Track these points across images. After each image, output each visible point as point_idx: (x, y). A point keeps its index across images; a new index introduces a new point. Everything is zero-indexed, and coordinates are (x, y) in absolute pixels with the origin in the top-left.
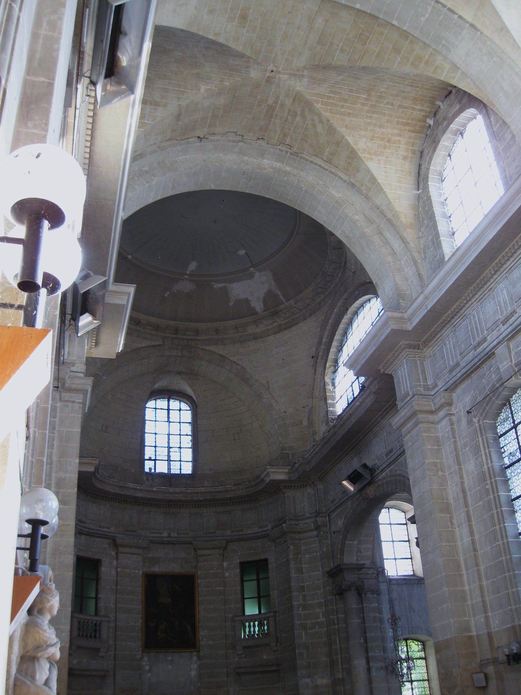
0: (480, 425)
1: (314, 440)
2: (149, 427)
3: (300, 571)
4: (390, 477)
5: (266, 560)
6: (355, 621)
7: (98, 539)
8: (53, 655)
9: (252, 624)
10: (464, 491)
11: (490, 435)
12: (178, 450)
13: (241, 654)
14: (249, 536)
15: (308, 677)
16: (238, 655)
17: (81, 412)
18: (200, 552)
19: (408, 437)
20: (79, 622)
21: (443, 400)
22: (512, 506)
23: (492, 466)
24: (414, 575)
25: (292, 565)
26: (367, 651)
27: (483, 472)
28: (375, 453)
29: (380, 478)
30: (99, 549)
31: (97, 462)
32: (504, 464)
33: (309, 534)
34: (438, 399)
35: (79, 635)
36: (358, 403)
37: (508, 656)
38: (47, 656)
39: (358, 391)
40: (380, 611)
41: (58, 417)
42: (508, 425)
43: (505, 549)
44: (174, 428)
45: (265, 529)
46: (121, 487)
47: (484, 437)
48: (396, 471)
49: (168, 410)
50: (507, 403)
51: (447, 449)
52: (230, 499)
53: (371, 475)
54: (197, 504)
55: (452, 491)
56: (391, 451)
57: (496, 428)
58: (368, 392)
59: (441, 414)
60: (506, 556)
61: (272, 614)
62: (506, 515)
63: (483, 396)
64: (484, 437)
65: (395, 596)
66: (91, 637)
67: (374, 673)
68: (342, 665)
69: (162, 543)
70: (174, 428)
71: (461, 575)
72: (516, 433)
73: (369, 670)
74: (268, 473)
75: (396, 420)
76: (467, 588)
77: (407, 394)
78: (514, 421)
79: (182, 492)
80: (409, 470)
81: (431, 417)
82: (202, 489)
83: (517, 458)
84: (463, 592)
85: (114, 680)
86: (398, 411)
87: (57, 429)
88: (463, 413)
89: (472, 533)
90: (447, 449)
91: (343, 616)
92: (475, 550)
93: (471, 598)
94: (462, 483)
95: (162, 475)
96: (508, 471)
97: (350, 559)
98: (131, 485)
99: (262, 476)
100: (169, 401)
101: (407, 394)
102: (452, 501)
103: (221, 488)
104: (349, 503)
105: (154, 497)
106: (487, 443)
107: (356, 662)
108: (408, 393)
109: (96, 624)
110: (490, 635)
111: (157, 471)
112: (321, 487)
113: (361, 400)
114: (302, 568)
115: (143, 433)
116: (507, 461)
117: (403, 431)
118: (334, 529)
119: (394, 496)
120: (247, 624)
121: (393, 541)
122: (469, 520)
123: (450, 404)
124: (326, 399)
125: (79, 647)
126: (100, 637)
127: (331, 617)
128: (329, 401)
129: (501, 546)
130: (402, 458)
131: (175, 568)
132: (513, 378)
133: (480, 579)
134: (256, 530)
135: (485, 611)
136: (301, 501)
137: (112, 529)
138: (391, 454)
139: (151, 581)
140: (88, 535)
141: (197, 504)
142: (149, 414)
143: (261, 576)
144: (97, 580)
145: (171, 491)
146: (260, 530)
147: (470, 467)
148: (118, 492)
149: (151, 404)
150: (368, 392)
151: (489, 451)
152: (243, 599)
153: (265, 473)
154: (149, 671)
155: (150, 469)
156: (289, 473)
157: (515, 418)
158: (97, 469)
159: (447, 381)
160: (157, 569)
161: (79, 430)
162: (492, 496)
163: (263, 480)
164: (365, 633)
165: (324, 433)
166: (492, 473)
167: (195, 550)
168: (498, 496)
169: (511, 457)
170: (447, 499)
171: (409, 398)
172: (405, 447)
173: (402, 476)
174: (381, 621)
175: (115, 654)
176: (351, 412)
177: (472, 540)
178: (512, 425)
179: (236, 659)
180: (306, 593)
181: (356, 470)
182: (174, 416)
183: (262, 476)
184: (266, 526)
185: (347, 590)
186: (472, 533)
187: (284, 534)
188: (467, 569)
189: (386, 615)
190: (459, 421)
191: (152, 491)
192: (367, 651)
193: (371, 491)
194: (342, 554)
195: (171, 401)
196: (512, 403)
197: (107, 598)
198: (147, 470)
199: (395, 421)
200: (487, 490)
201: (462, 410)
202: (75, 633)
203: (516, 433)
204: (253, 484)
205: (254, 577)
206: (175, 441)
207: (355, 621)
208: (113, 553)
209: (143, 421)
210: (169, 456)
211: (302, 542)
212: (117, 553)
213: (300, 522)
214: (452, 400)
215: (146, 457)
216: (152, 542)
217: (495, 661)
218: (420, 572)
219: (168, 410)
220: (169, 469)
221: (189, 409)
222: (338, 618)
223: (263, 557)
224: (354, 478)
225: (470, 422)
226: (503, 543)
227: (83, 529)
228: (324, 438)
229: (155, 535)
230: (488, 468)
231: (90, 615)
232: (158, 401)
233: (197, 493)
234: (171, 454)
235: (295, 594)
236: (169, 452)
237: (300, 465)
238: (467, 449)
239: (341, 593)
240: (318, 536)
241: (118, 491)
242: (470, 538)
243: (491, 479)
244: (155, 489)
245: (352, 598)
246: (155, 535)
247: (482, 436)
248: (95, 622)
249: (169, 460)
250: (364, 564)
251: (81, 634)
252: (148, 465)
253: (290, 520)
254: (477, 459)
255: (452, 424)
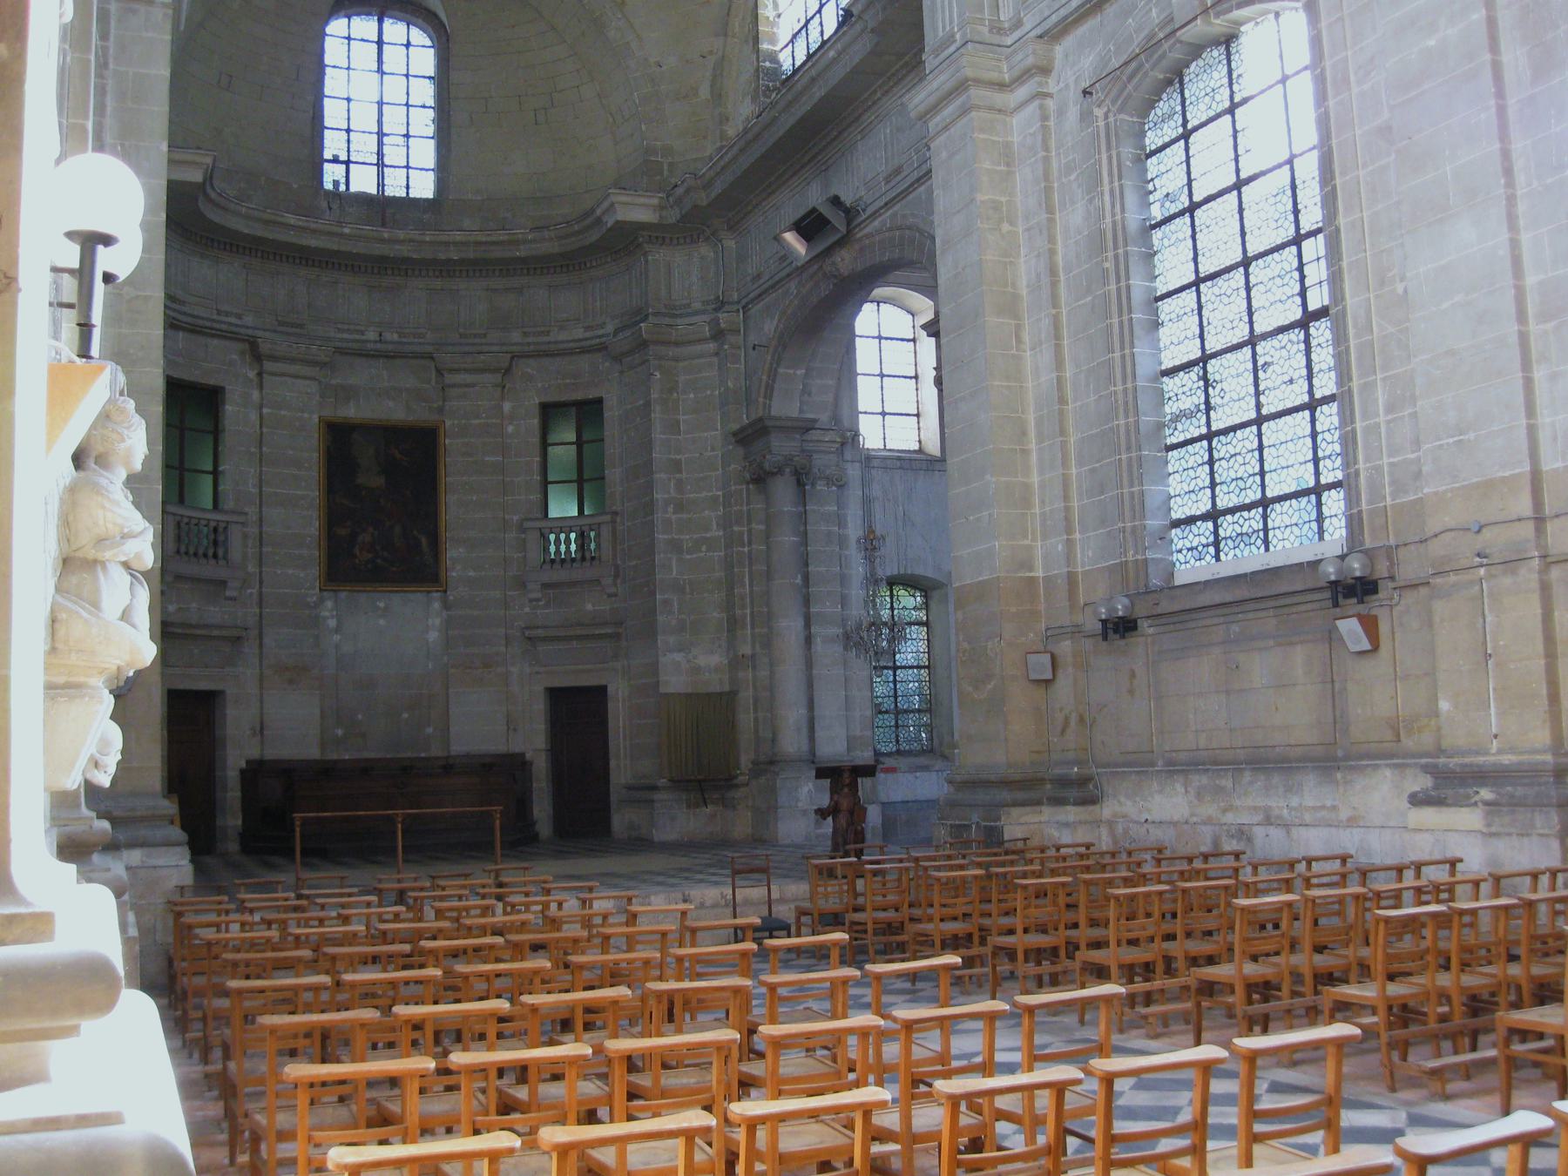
0: (1107, 125)
1: (723, 136)
2: (333, 83)
3: (674, 427)
4: (890, 229)
5: (600, 401)
6: (786, 538)
7: (216, 341)
8: (138, 556)
9: (563, 536)
10: (1053, 272)
11: (1128, 151)
12: (401, 140)
13: (538, 600)
14: (562, 346)
15: (680, 651)
16: (531, 601)
17: (168, 26)
18: (450, 378)
19: (942, 138)
20: (178, 524)
21: (1030, 60)
22: (1156, 312)
23: (1123, 219)
24: (920, 451)
25: (657, 414)
26: (807, 602)
27: (1102, 233)
28: (860, 174)
29: (866, 231)
30: (216, 364)
31: (209, 160)
32: (1149, 219)
33: (698, 348)
34: (1019, 57)
35: (178, 552)
36: (832, 54)
37: (1104, 622)
38: (123, 559)
39: (835, 25)
40: (841, 523)
41: (112, 39)
42: (1171, 130)
43: (1126, 403)
44: (394, 89)
45: (601, 332)
46: (267, 222)
47: (1114, 153)
48: (904, 216)
49: (380, 43)
50: (1176, 78)
51: (1025, 176)
52: (523, 260)
53: (848, 224)
54: (445, 269)
55: (1025, 270)
56: (898, 171)
57: (1143, 134)
58: (858, 27)
59: (1022, 92)
60: (1127, 417)
61: (607, 518)
62: (1138, 331)
63: (1124, 58)
64: (1114, 153)
65: (876, 491)
66: (205, 555)
67: (818, 646)
68: (753, 628)
69: (364, 354)
70: (394, 89)
71: (1025, 452)
72: (1187, 149)
73: (809, 640)
74: (612, 205)
75: (919, 98)
76: (1035, 479)
77: (951, 38)
78: (1185, 122)
79: (411, 241)
80: (936, 219)
81: (999, 99)
82: (458, 236)
83: (1181, 207)
84: (1027, 487)
85: (261, 645)
86: (921, 80)
87: (111, 66)
88: (1074, 94)
89: (1059, 364)
90: (1025, 176)
91: (762, 527)
92: (1062, 400)
93: (1043, 502)
94: (1052, 252)
95: (363, 198)
96: (1157, 235)
97: (784, 407)
98: (291, 219)
99: (598, 212)
100: (380, 22)
101: (951, 38)
102: (1024, 292)
103: (502, 236)
104: (792, 286)
105: (343, 248)
106: (1119, 165)
107: (783, 623)
108: (953, 36)
109: (215, 530)
110: (1071, 579)
111: (353, 189)
112: (730, 244)
113: (839, 46)
114: (678, 422)
115: (319, 96)
116: (1157, 213)
117: (931, 125)
118: (753, 339)
119: (891, 277)
120: (552, 537)
121: (882, 376)
122: (1058, 337)
123: (1045, 71)
124: (756, 40)
125: (179, 577)
126: (225, 558)
127: (736, 529)
128: (764, 46)
129: (1120, 396)
130: (922, 188)
131: (394, 411)
132: (1198, 21)
133: (1065, 463)
134: (579, 333)
135: (1069, 530)
136: (684, 274)
137: (249, 320)
138: (899, 178)
139: (341, 441)
140: (192, 331)
141: (445, 269)
142: (333, 51)
143: (586, 436)
144: (216, 432)
145: (386, 235)
146: (588, 335)
147: (1074, 218)
148: (259, 233)
149: (337, 26)
150: (858, 27)
151: (1121, 186)
152: (545, 483)
153: (606, 204)
154: (337, 630)
155: (336, 183)
156: (662, 208)
157: (1189, 116)
158: (209, 178)
159: (1047, 13)
160: (351, 412)
161: (166, 72)
162: (1113, 287)
163: (599, 221)
164: (807, 565)
165: (747, 120)
166: (1120, 233)
167: (439, 372)
168: (1128, 287)
169: (1167, 204)
170: (1014, 285)
171: (952, 49)
172: (934, 163)
173: (921, 232)
174: (842, 541)
175: (261, 594)
176: (813, 72)
177: (1059, 379)
178: (1181, 130)
179: (527, 610)
180: (684, 475)
181: (814, 210)
182: (394, 58)
183: (598, 212)
184: (602, 326)
185: (774, 474)
186: (1059, 364)
187: (644, 344)
188: (1041, 438)
189: (854, 531)
190: (1061, 112)
191: (342, 235)
192: (807, 602)
193: (845, 261)
194: (769, 391)
195: (387, 23)
196: (1186, 79)
197: (239, 472)
198: (328, 186)
199: (916, 101)
200: (1105, 272)
201: (1072, 87)
202: (172, 546)
203: (1187, 149)
204: (576, 228)
205: (572, 437)
206: (394, 120)
207: (786, 538)
208: (252, 374)
209: (321, 67)
210: (380, 154)
211: (681, 364)
212: (260, 374)
213: (679, 321)
214: (1051, 60)
215: (327, 155)
216: (341, 351)
217: (1076, 631)
218: (933, 447)
219: (380, 43)
220: (381, 185)
221: (429, 43)
222: (750, 531)
223: (592, 394)
224: (810, 226)
225: (1086, 117)
226: (1125, 390)
227: (180, 317)
228: (746, 131)
229: (345, 336)
230: (1114, 223)
231: (203, 510)
232: (356, 21)
233: (447, 244)
234: (386, 150)
235: (660, 476)
236: (380, 144)
237: (688, 191)
238: (1072, 177)
239: (760, 479)
240: (717, 354)
241: (260, 231)
242: (1054, 375)
243: (1116, 248)
244: (347, 231)
245: (783, 490)
246: (345, 336)
247: (1109, 148)
248: (213, 524)
249: (380, 164)
250: (815, 421)
251: (183, 549)
252: (332, 174)
253: (656, 314)
254: (1091, 201)
255: (1045, 118)
